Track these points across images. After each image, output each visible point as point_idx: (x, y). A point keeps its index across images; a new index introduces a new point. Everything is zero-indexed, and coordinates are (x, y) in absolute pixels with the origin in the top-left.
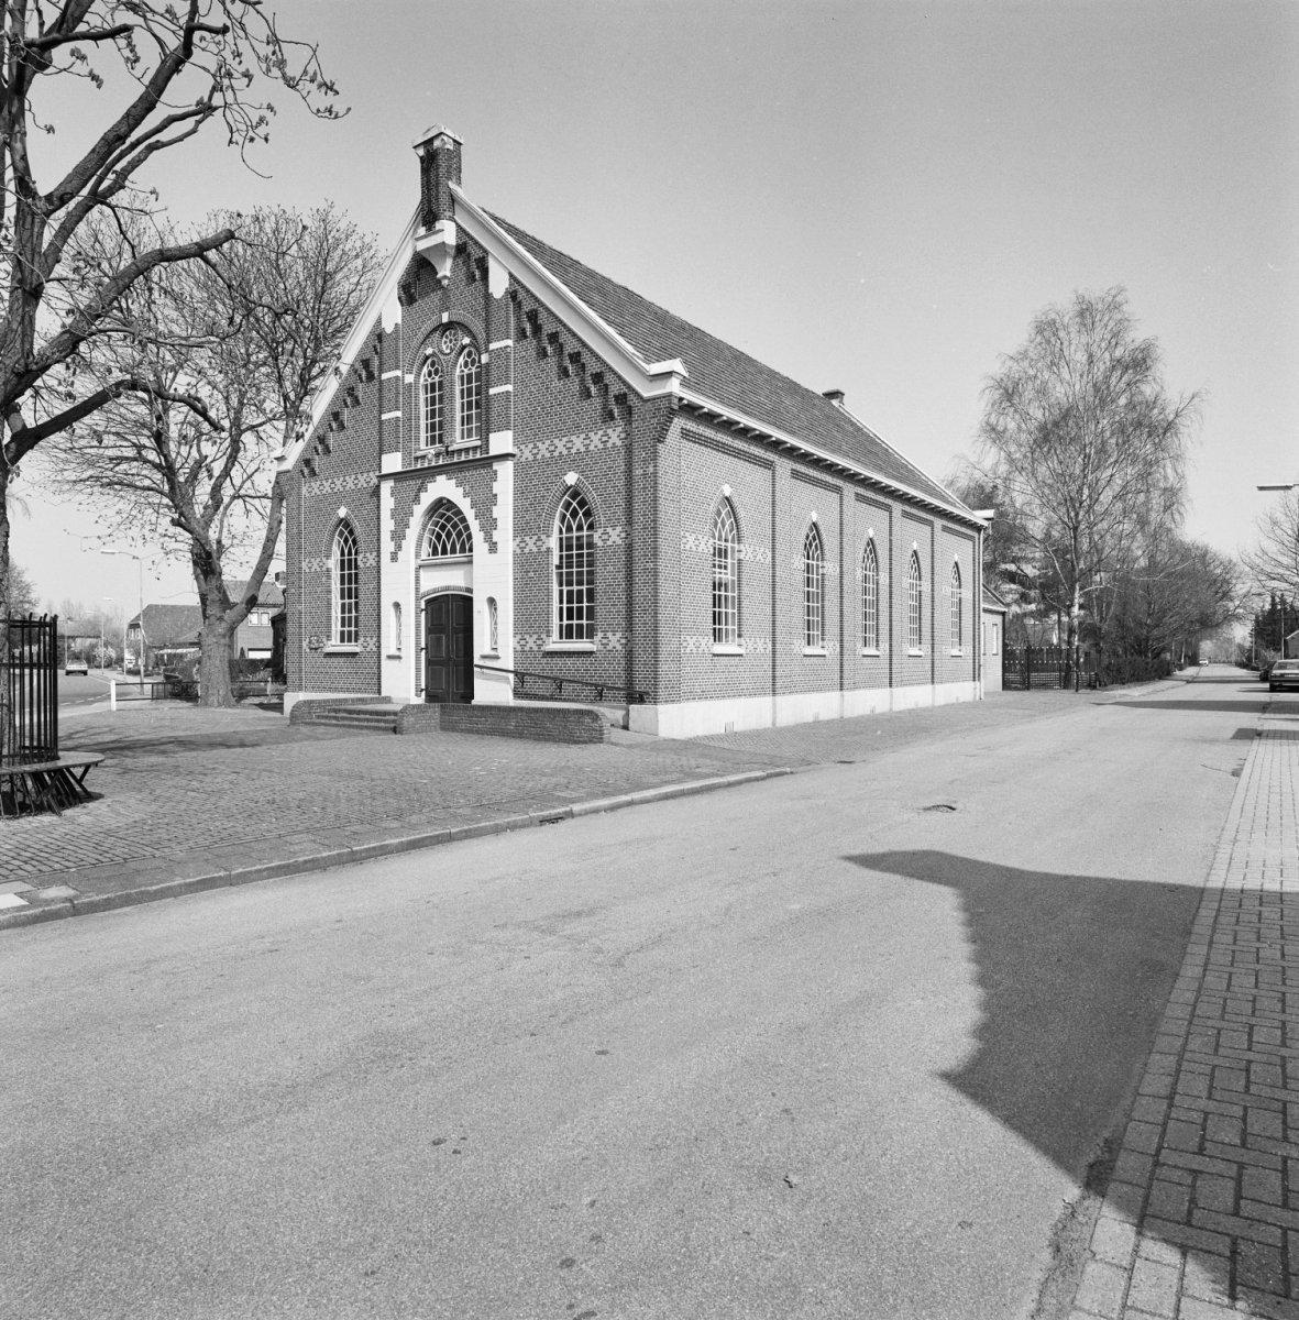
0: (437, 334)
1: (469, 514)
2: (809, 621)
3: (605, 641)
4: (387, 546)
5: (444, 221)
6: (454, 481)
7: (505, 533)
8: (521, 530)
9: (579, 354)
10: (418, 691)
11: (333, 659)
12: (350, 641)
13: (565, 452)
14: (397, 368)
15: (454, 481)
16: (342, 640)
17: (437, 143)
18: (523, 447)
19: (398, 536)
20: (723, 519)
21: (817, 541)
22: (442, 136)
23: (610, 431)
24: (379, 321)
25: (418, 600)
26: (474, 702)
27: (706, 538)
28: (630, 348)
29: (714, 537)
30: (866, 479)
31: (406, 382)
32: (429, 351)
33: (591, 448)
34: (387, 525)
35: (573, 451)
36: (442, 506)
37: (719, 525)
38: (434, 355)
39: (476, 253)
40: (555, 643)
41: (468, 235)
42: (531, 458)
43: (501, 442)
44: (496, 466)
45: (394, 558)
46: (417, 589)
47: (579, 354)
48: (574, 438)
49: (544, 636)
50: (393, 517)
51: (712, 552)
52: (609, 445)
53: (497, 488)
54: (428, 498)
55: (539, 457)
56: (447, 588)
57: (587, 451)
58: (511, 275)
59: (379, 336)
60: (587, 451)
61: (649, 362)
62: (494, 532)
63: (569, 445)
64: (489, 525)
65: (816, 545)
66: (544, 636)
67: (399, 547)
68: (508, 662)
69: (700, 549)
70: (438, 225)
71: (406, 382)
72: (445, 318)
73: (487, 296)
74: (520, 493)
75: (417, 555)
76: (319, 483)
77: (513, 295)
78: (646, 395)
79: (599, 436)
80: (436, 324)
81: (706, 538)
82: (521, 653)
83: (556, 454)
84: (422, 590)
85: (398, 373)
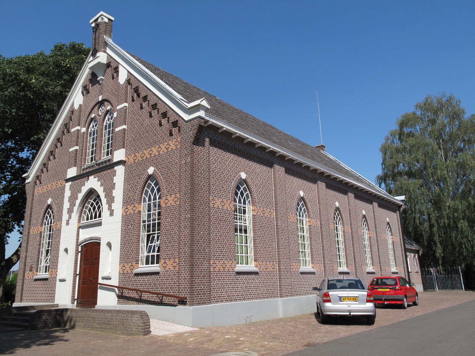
0: (97, 107)
1: (102, 195)
2: (304, 241)
3: (165, 265)
4: (65, 216)
5: (100, 53)
6: (97, 178)
7: (118, 205)
8: (127, 202)
9: (156, 104)
10: (73, 300)
11: (37, 282)
12: (152, 263)
13: (149, 156)
14: (79, 125)
15: (97, 178)
16: (147, 263)
17: (99, 20)
18: (129, 157)
19: (70, 211)
20: (300, 207)
21: (340, 216)
22: (102, 16)
23: (170, 142)
24: (73, 104)
25: (77, 246)
26: (97, 307)
27: (229, 202)
28: (179, 96)
29: (235, 201)
30: (329, 176)
31: (82, 132)
32: (93, 116)
33: (161, 152)
34: (66, 205)
35: (153, 155)
36: (91, 193)
37: (299, 209)
38: (95, 117)
39: (113, 65)
40: (143, 268)
41: (112, 57)
42: (133, 162)
43: (119, 155)
44: (116, 168)
45: (67, 224)
46: (78, 240)
47: (156, 104)
48: (153, 148)
49: (134, 264)
50: (69, 201)
51: (233, 209)
52: (170, 150)
53: (116, 180)
54: (85, 189)
55: (136, 161)
56: (91, 239)
57: (159, 154)
58: (128, 72)
59: (72, 111)
60: (159, 154)
61: (189, 102)
62: (113, 204)
63: (151, 152)
64: (111, 200)
65: (339, 218)
66: (134, 264)
67: (70, 217)
68: (115, 282)
69: (225, 207)
70: (98, 54)
71: (82, 132)
72: (100, 98)
73: (118, 84)
74: (127, 180)
75: (79, 221)
76: (42, 187)
77: (128, 82)
78: (186, 119)
79: (170, 148)
80: (96, 102)
81: (229, 202)
82: (123, 275)
83: (144, 158)
84: (80, 241)
85: (78, 128)
